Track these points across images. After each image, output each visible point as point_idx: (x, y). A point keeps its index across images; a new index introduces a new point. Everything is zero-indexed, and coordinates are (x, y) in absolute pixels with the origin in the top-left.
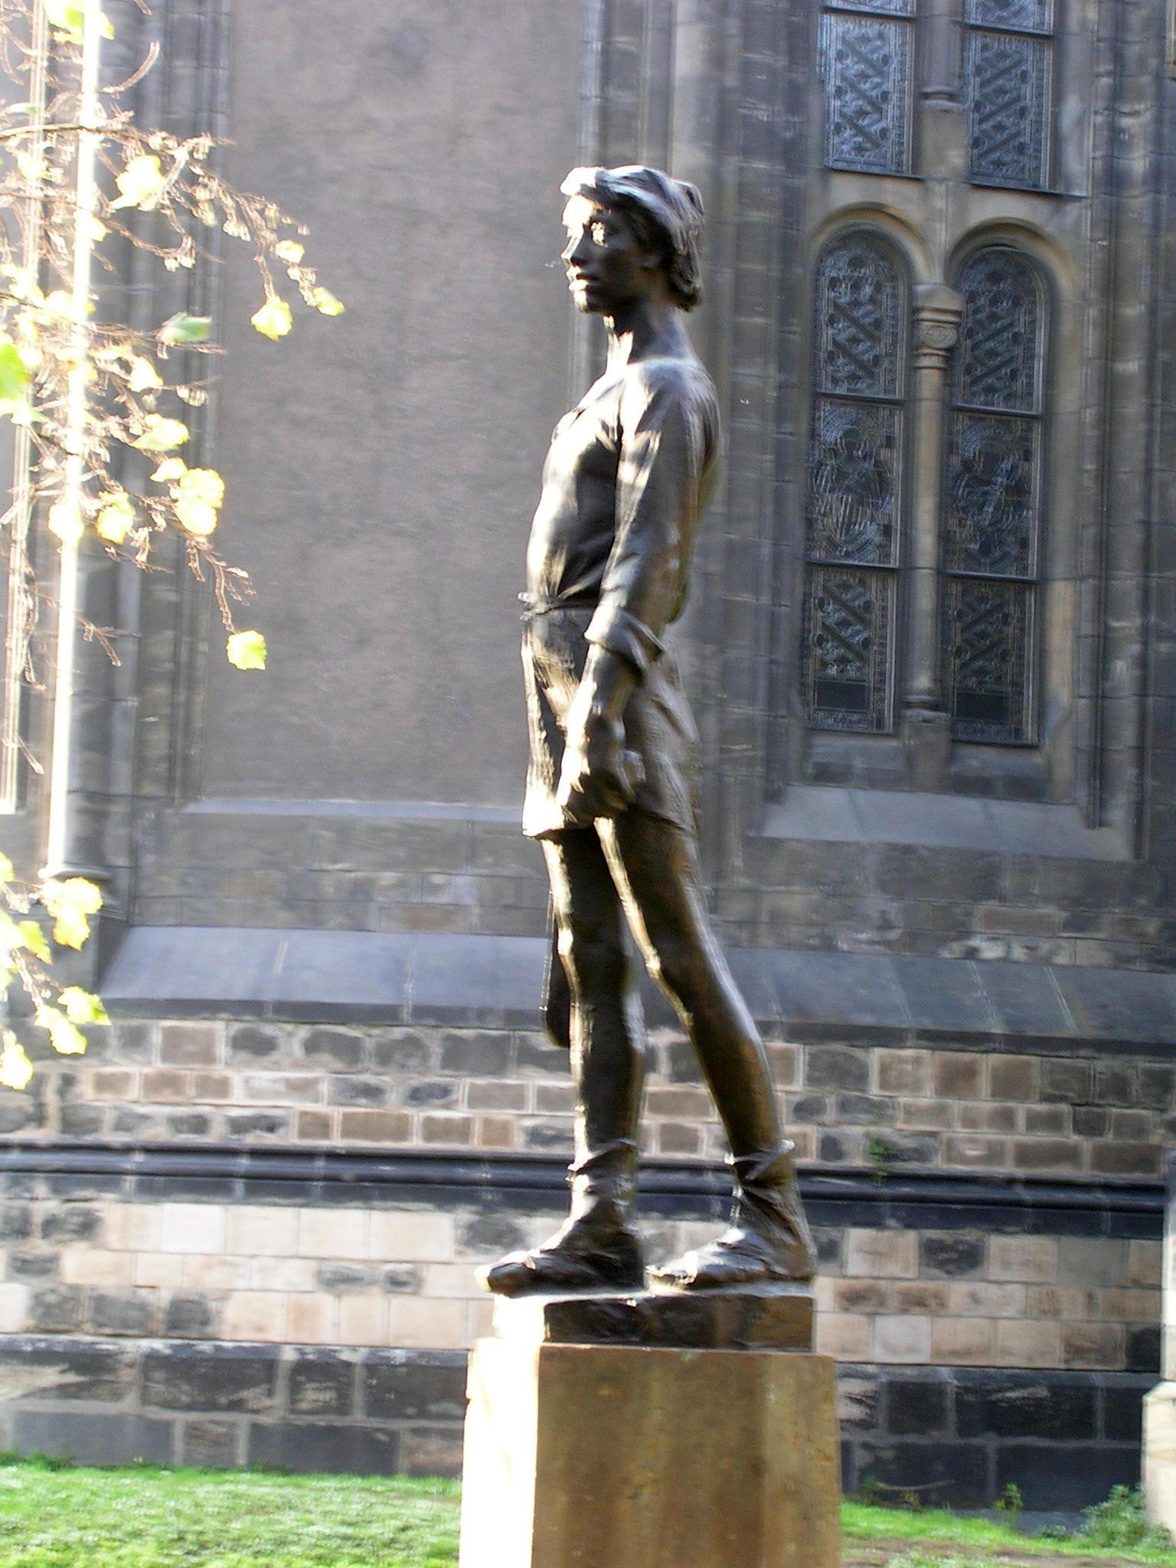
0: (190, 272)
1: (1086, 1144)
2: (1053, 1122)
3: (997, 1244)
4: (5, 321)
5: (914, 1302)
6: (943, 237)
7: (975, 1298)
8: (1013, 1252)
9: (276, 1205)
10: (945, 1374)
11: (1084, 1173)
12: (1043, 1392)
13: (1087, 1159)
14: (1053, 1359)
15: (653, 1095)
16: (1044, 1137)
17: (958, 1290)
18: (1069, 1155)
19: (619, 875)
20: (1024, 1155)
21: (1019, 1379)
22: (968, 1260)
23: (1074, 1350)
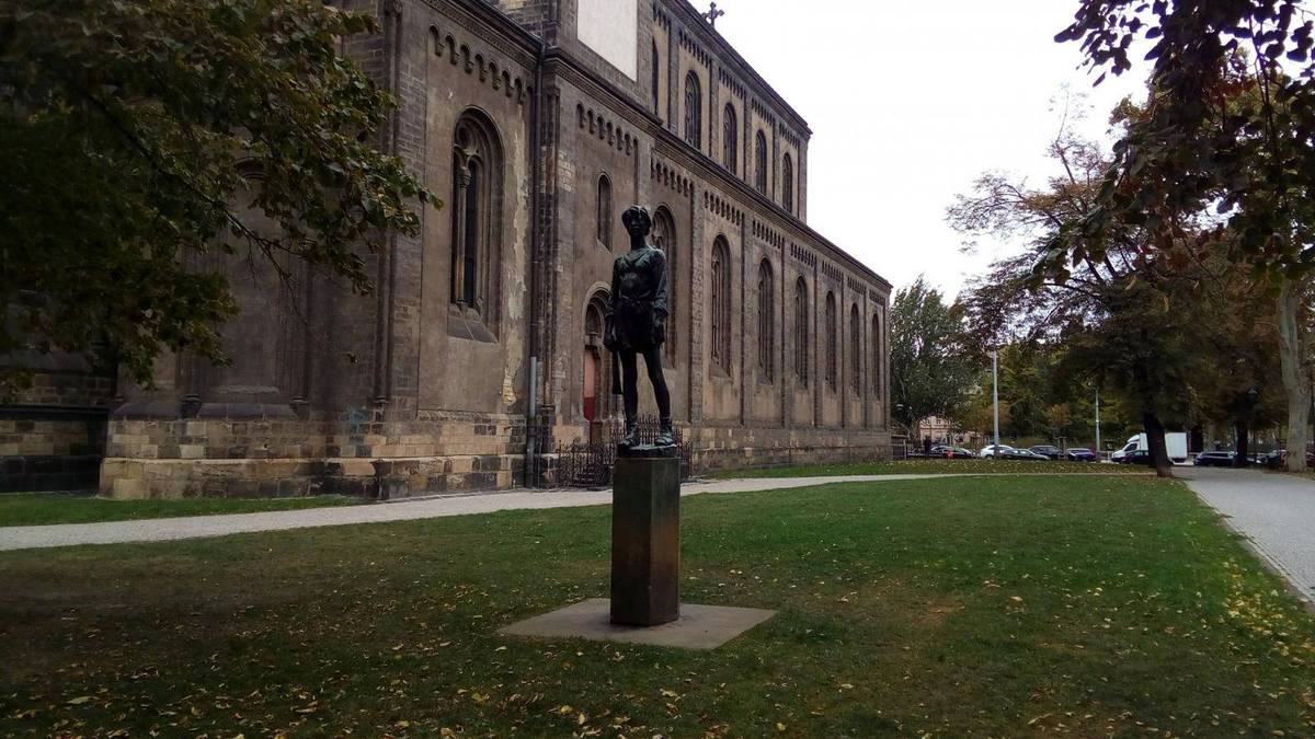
0: (1172, 107)
1: (59, 397)
2: (51, 391)
3: (37, 424)
4: (1310, 41)
5: (14, 440)
6: (626, 208)
7: (31, 438)
8: (42, 427)
9: (336, 504)
10: (22, 458)
11: (59, 404)
12: (48, 461)
13: (60, 400)
14: (50, 452)
15: (690, 498)
16: (49, 395)
17: (26, 436)
18: (55, 400)
19: (942, 476)
20: (43, 400)
21: (41, 458)
22: (29, 428)
23: (55, 449)
